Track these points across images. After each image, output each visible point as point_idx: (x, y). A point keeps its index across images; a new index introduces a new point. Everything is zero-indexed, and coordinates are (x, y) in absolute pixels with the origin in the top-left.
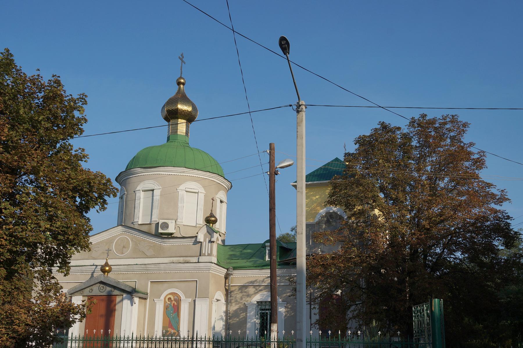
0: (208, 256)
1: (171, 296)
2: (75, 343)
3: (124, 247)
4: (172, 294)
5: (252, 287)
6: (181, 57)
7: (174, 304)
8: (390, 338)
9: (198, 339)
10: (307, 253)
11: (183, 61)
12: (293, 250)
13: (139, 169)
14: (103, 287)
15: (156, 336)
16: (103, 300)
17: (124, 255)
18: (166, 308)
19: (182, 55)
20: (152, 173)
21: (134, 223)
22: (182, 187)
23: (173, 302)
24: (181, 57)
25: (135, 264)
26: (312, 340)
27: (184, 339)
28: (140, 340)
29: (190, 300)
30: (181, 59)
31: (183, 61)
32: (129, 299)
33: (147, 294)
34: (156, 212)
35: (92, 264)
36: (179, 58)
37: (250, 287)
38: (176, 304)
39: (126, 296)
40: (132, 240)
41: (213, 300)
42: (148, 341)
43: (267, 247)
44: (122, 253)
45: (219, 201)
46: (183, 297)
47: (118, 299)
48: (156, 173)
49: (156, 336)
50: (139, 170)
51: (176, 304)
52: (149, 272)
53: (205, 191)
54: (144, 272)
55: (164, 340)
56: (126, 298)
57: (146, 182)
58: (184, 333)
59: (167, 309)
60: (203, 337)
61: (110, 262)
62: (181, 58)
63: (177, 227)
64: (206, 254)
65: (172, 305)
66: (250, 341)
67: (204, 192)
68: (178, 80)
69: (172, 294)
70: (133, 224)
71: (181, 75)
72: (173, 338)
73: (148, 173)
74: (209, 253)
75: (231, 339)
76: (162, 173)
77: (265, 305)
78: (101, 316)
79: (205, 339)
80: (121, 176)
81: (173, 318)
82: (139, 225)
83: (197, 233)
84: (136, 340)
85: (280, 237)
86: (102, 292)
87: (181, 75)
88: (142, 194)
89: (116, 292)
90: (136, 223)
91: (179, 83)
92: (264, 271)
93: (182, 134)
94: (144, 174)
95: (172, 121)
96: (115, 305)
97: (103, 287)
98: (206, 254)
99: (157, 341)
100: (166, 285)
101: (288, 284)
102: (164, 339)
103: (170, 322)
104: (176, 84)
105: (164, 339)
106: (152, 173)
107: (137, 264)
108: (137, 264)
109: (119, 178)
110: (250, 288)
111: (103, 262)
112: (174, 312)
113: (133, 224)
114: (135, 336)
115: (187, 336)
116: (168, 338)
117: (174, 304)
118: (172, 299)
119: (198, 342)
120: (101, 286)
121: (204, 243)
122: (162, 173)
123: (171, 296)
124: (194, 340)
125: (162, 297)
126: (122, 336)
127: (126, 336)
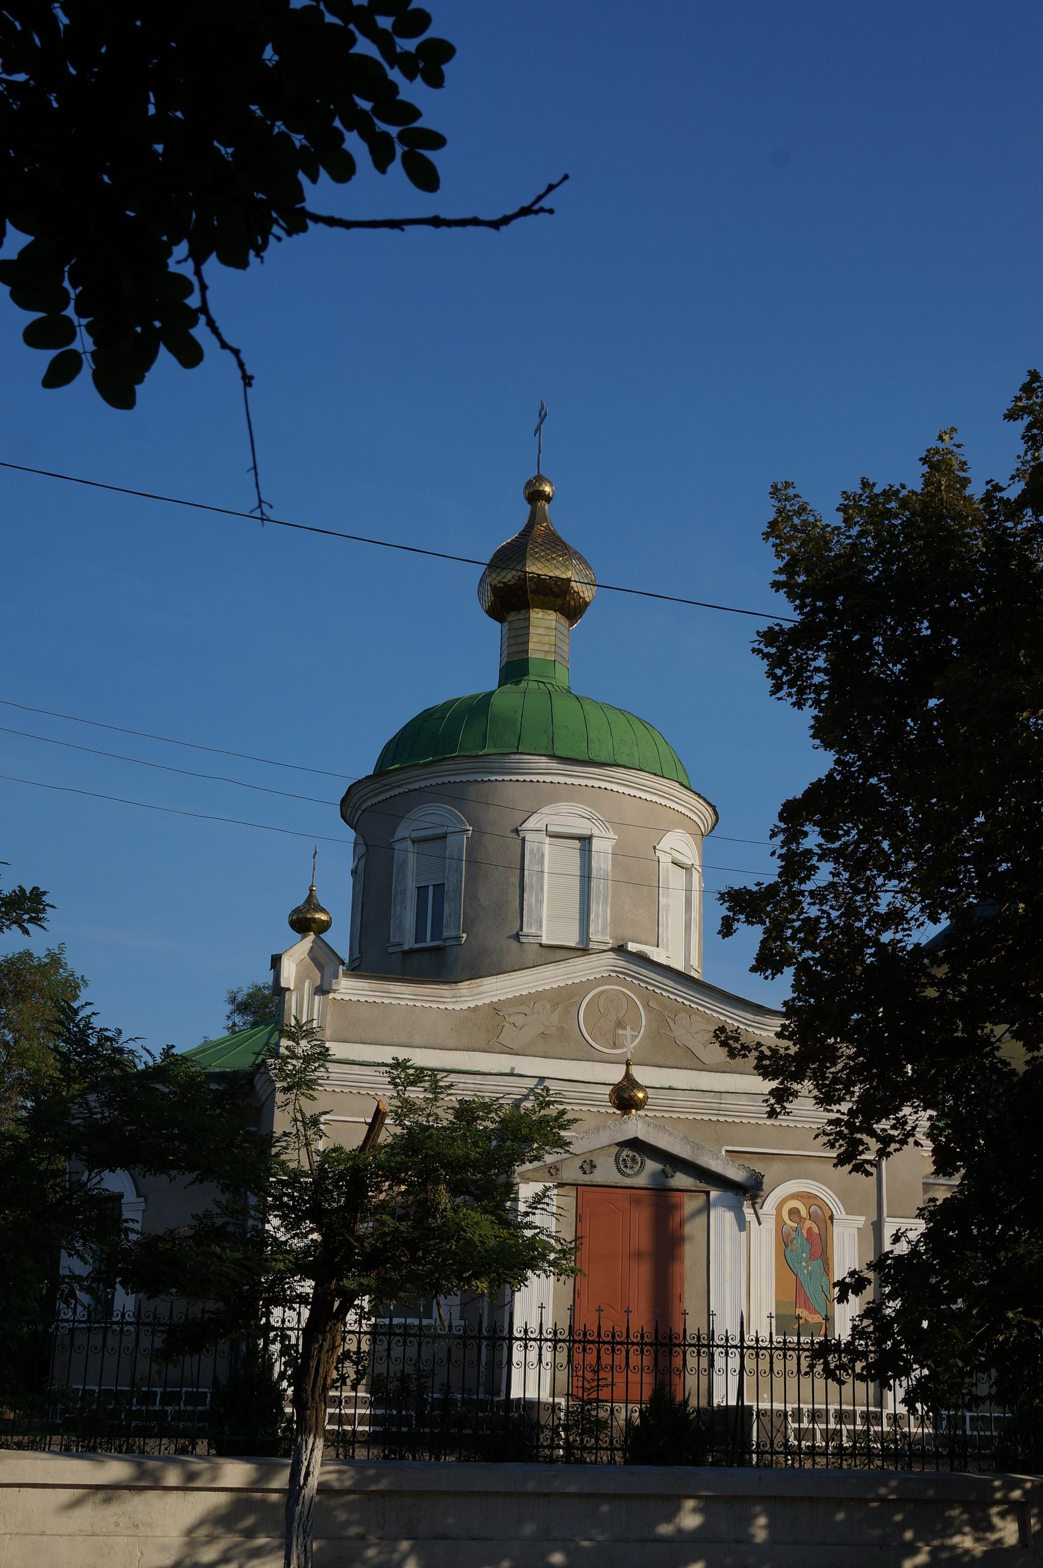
1: (796, 1204)
2: (699, 1354)
4: (803, 1197)
5: (944, 1188)
7: (810, 1230)
13: (544, 759)
14: (634, 1160)
16: (636, 1201)
18: (784, 1241)
20: (583, 782)
21: (523, 940)
23: (808, 1224)
25: (667, 1086)
29: (860, 1221)
32: (730, 1208)
34: (599, 912)
35: (508, 1071)
37: (937, 1187)
38: (816, 1230)
39: (718, 1199)
40: (647, 1006)
44: (615, 1046)
47: (691, 1204)
48: (597, 784)
50: (543, 762)
51: (816, 1230)
52: (722, 1119)
54: (706, 1118)
56: (719, 1202)
57: (564, 807)
59: (786, 1246)
60: (620, 1329)
61: (642, 1075)
65: (805, 1232)
66: (635, 1341)
68: (529, 484)
69: (803, 1197)
70: (519, 941)
72: (802, 1339)
73: (569, 780)
76: (615, 788)
78: (639, 1255)
79: (541, 1333)
80: (436, 768)
81: (810, 1274)
82: (541, 945)
84: (556, 1341)
86: (628, 1176)
88: (548, 846)
89: (681, 1180)
90: (532, 940)
91: (534, 496)
94: (556, 779)
95: (512, 617)
96: (682, 1224)
97: (634, 1160)
99: (776, 1349)
102: (799, 1343)
103: (799, 1287)
105: (799, 1343)
106: (583, 782)
107: (674, 1086)
110: (937, 1190)
111: (615, 1074)
112: (812, 1257)
113: (519, 941)
114: (548, 1325)
116: (785, 1340)
117: (810, 1230)
118: (804, 1212)
120: (624, 1154)
122: (615, 788)
123: (796, 1204)
124: (368, 1337)
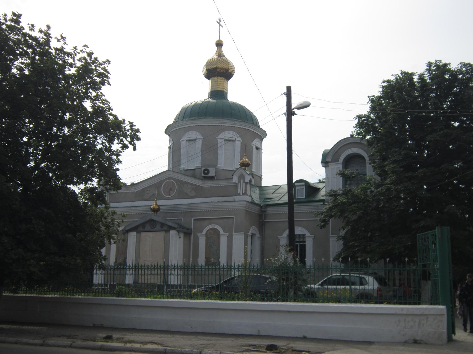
0: (242, 195)
3: (171, 189)
6: (219, 21)
8: (115, 340)
10: (207, 67)
11: (220, 25)
12: (321, 189)
15: (235, 264)
22: (221, 136)
24: (219, 21)
26: (333, 266)
27: (224, 266)
29: (227, 234)
30: (219, 23)
31: (220, 25)
36: (217, 22)
41: (248, 234)
42: (157, 268)
43: (296, 187)
44: (169, 195)
46: (222, 232)
49: (235, 264)
53: (242, 139)
55: (205, 268)
58: (223, 261)
63: (217, 171)
64: (241, 194)
67: (240, 140)
71: (219, 38)
74: (244, 192)
77: (299, 238)
80: (169, 129)
87: (219, 38)
93: (210, 82)
98: (241, 194)
100: (207, 222)
115: (157, 264)
121: (239, 184)
125: (204, 232)
126: (170, 264)
127: (173, 264)
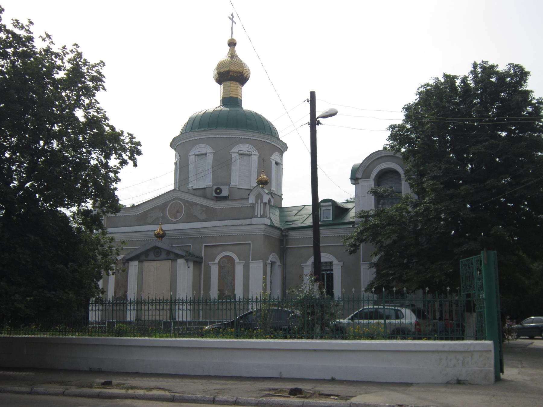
0: (260, 217)
3: (178, 212)
6: (231, 17)
9: (365, 299)
11: (233, 21)
12: (350, 209)
17: (177, 220)
19: (232, 15)
22: (235, 150)
24: (231, 17)
28: (252, 302)
29: (243, 262)
30: (232, 19)
31: (233, 21)
33: (202, 258)
36: (229, 18)
44: (176, 218)
45: (273, 162)
46: (237, 260)
55: (218, 302)
58: (239, 293)
62: (232, 18)
64: (259, 216)
67: (257, 154)
71: (232, 37)
74: (262, 214)
75: (364, 297)
83: (249, 195)
85: (123, 205)
87: (232, 37)
92: (277, 231)
98: (259, 216)
100: (220, 249)
101: (342, 244)
104: (228, 46)
108: (233, 225)
109: (174, 144)
119: (365, 302)
121: (257, 205)
125: (217, 261)
126: (177, 298)
